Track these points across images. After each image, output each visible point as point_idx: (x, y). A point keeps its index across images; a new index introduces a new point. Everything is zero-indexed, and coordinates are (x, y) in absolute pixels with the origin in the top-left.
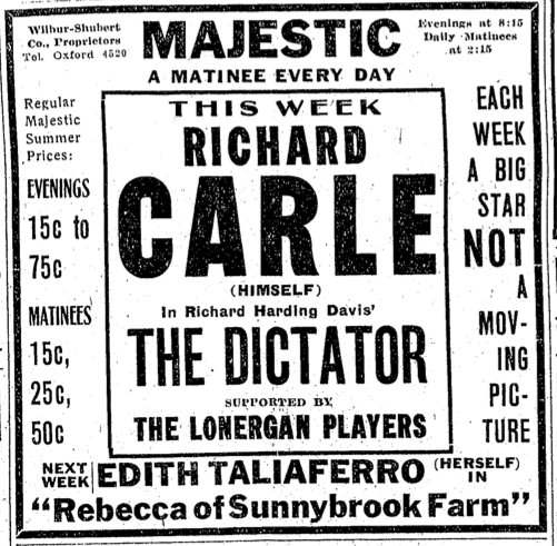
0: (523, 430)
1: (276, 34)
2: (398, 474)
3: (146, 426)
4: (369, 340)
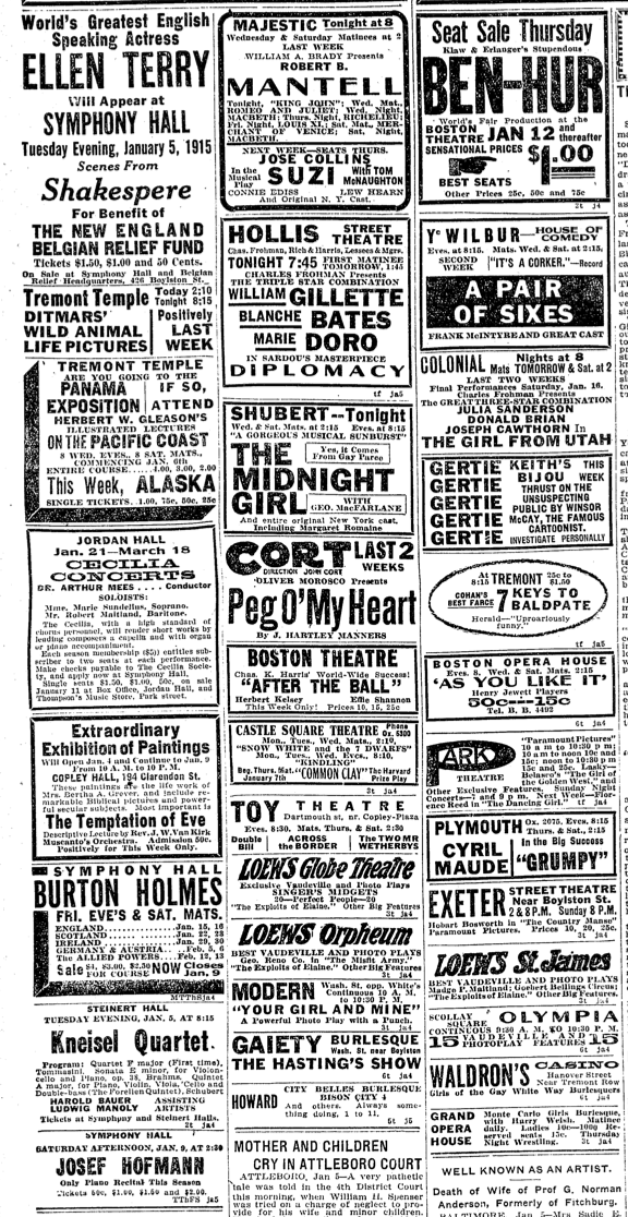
1: (375, 317)
2: (359, 344)
3: (41, 230)
4: (88, 887)
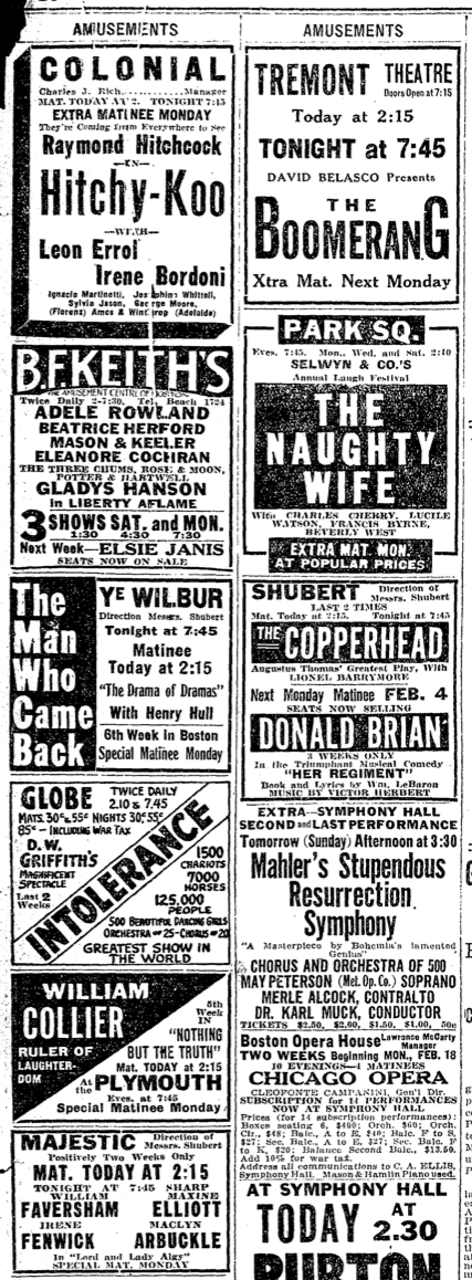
0: (446, 73)
1: (81, 1140)
2: (121, 414)
